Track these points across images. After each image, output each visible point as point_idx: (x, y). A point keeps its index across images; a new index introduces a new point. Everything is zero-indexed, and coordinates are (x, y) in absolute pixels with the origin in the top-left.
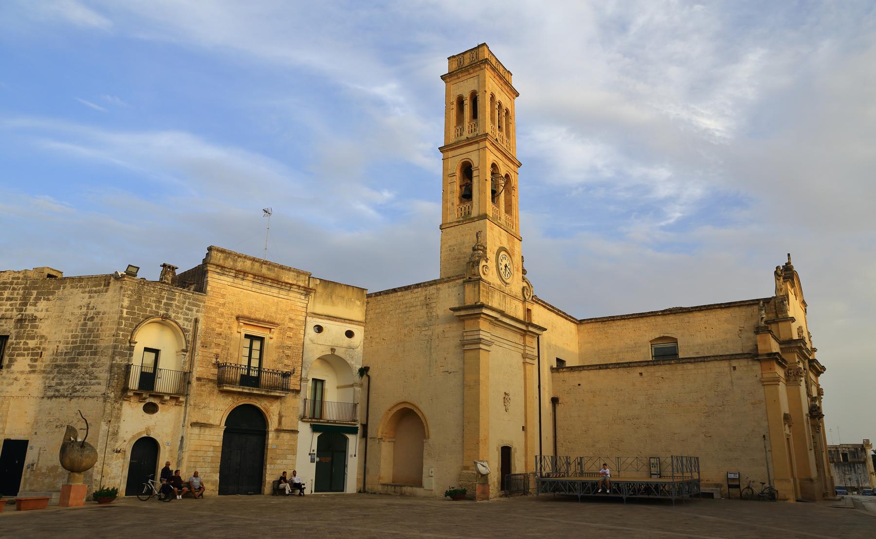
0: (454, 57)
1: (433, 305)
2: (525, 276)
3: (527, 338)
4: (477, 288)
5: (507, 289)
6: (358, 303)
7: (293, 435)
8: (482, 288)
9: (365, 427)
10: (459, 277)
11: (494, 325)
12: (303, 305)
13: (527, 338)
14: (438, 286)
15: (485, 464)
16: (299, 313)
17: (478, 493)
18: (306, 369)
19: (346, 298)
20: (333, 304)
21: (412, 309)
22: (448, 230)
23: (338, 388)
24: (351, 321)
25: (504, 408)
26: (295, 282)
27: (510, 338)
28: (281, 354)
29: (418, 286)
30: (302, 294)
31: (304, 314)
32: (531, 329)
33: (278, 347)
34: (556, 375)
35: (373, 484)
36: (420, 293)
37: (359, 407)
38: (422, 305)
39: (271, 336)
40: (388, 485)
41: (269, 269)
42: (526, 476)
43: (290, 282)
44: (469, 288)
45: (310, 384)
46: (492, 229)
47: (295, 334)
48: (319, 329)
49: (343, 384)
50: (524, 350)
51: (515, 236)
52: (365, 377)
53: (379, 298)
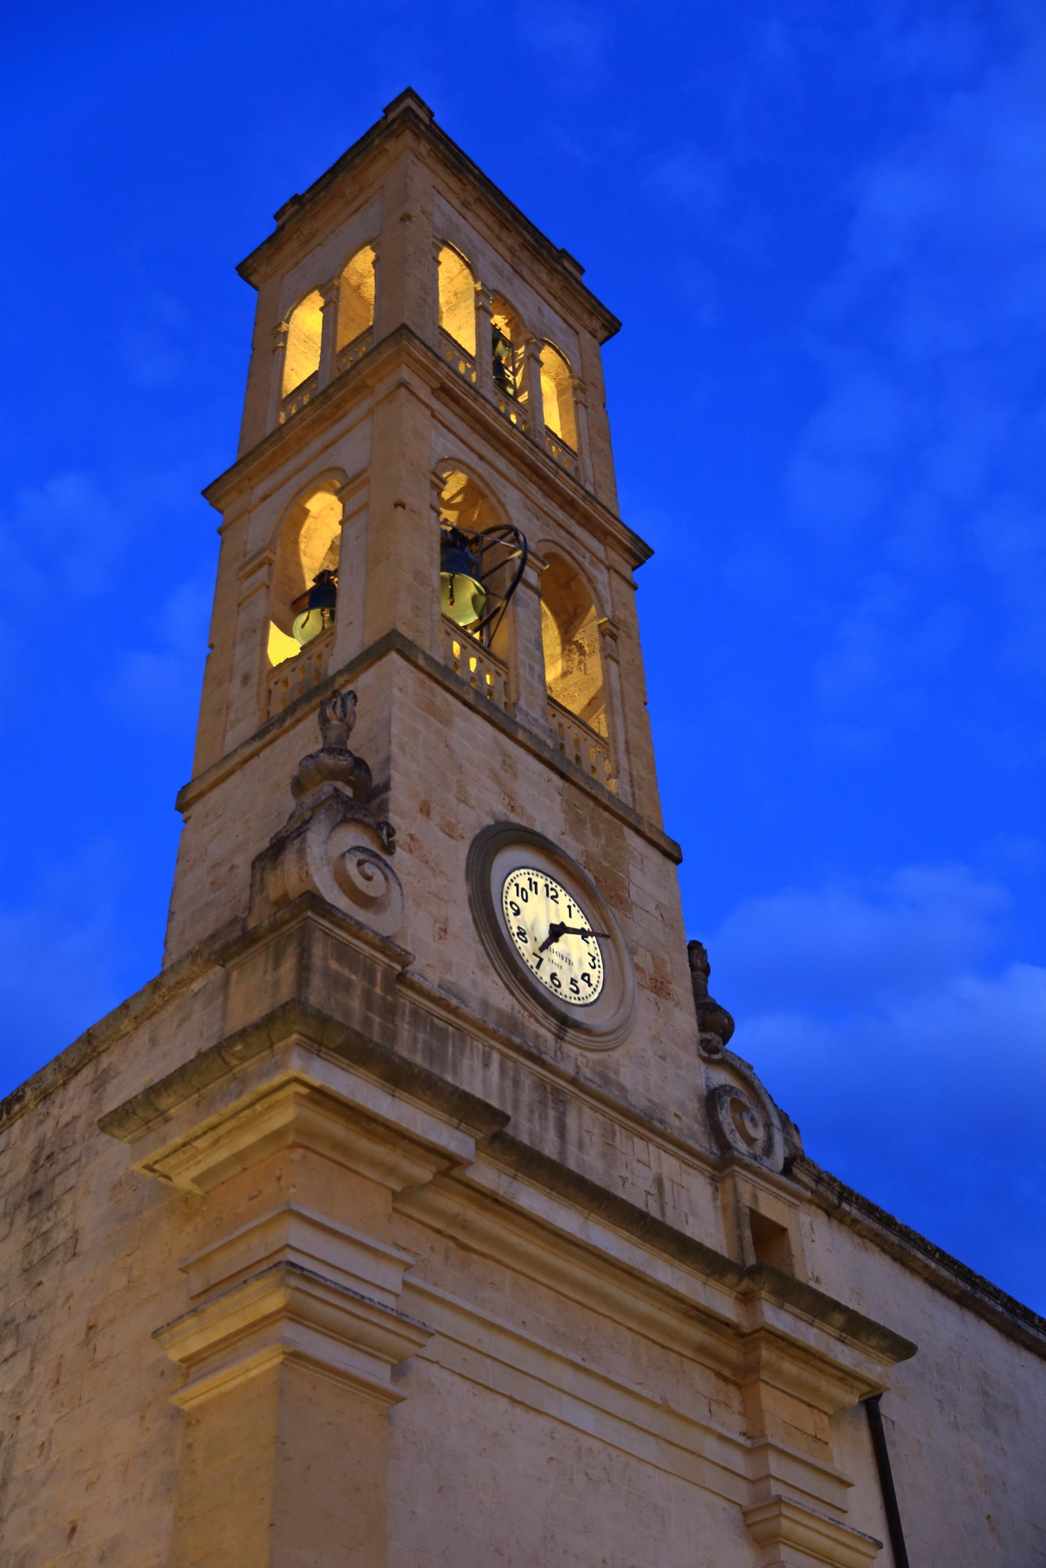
22: (215, 795)
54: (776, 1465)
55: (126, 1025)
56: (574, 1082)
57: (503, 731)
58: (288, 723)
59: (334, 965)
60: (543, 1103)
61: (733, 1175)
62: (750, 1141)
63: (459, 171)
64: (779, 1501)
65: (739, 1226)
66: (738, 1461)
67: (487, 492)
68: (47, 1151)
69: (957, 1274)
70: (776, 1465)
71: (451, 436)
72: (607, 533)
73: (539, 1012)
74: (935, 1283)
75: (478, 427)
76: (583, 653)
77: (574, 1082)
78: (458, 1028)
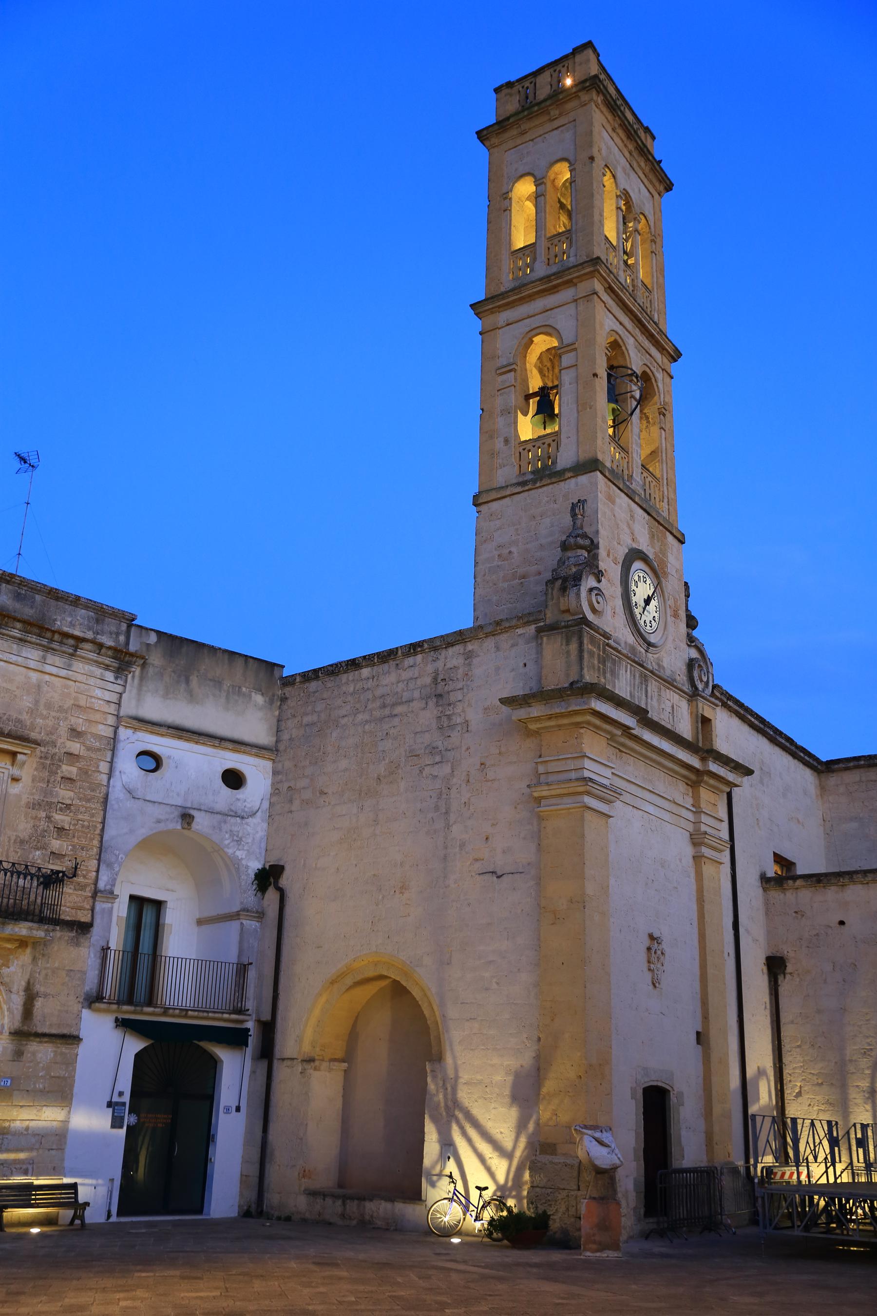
0: (510, 85)
1: (453, 697)
2: (695, 633)
3: (705, 794)
4: (574, 646)
5: (651, 660)
6: (259, 699)
7: (64, 1049)
8: (587, 646)
9: (268, 1029)
10: (525, 619)
11: (620, 749)
12: (108, 696)
13: (705, 794)
14: (470, 647)
15: (606, 1137)
16: (98, 717)
17: (586, 1227)
18: (110, 865)
19: (227, 684)
20: (192, 697)
21: (399, 709)
22: (495, 505)
23: (200, 922)
24: (238, 745)
25: (648, 976)
26: (89, 635)
27: (661, 788)
28: (43, 824)
29: (414, 648)
30: (107, 668)
31: (111, 720)
32: (714, 767)
33: (35, 805)
34: (776, 895)
35: (288, 1191)
36: (421, 669)
37: (252, 974)
38: (426, 698)
39: (16, 772)
40: (324, 1196)
41: (18, 597)
42: (708, 1175)
43: (77, 633)
44: (552, 646)
45: (121, 909)
46: (611, 499)
47: (84, 772)
48: (153, 761)
49: (213, 913)
50: (697, 823)
51: (665, 527)
52: (272, 895)
53: (313, 685)
54: (704, 818)
55: (481, 635)
56: (652, 672)
57: (631, 498)
58: (538, 485)
59: (590, 647)
60: (641, 683)
61: (696, 700)
62: (701, 681)
63: (614, 110)
64: (706, 833)
65: (697, 722)
66: (690, 816)
67: (621, 344)
68: (441, 677)
69: (760, 722)
70: (704, 818)
71: (610, 315)
72: (664, 349)
73: (642, 642)
74: (752, 726)
75: (620, 304)
76: (648, 422)
77: (652, 672)
78: (619, 658)
